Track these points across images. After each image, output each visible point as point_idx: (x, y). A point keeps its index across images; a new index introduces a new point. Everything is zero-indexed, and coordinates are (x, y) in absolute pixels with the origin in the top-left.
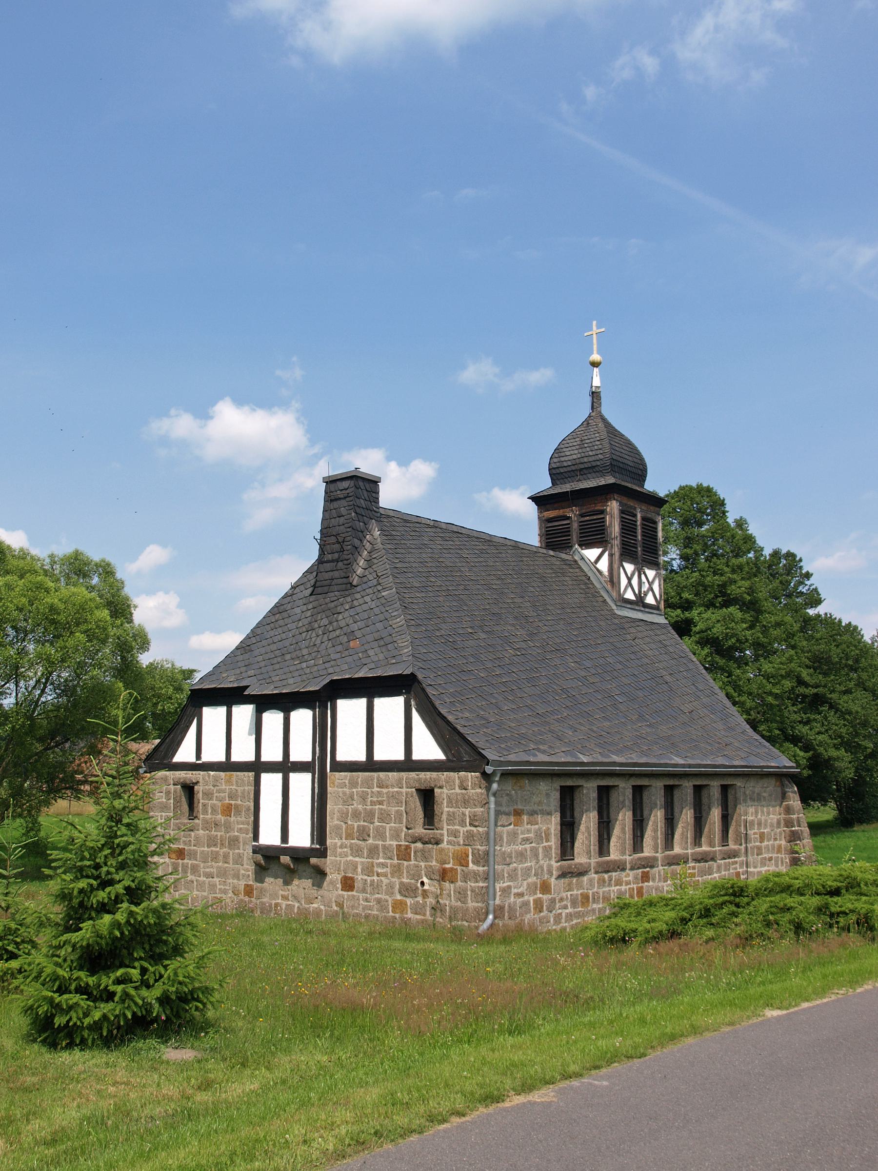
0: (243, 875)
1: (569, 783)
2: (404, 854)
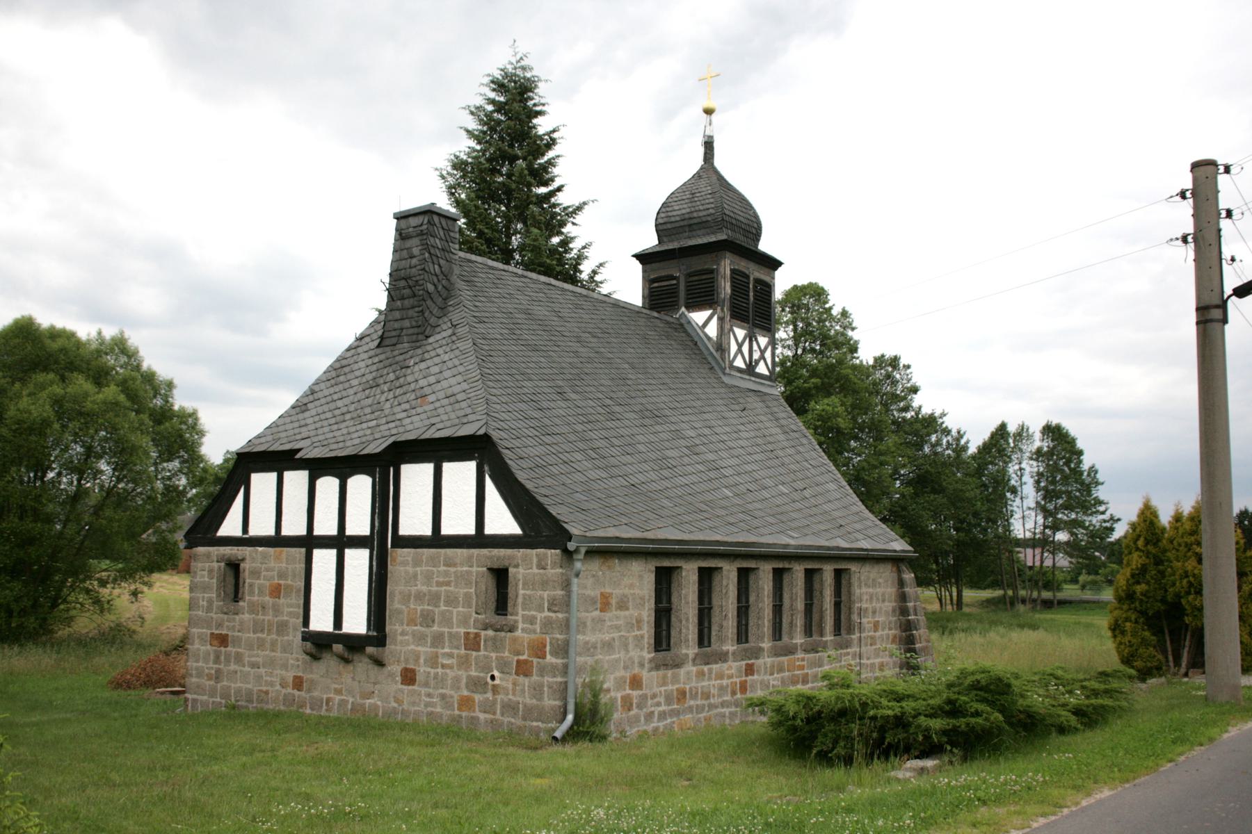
0: (293, 665)
1: (666, 563)
2: (472, 643)
